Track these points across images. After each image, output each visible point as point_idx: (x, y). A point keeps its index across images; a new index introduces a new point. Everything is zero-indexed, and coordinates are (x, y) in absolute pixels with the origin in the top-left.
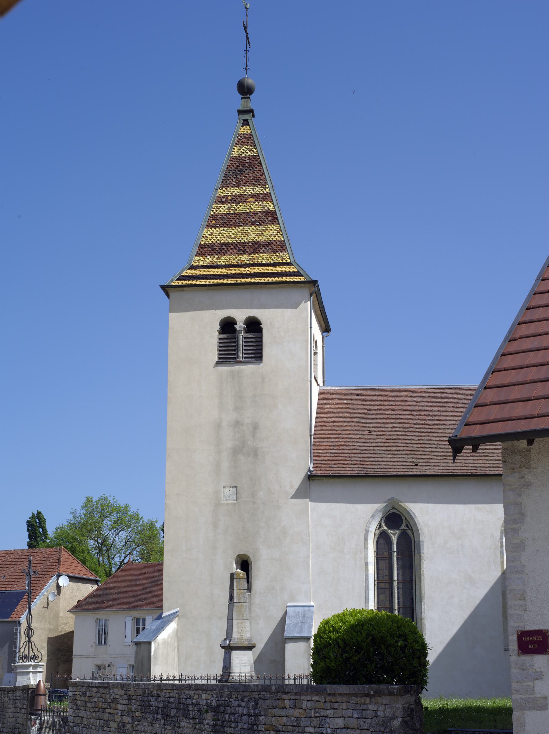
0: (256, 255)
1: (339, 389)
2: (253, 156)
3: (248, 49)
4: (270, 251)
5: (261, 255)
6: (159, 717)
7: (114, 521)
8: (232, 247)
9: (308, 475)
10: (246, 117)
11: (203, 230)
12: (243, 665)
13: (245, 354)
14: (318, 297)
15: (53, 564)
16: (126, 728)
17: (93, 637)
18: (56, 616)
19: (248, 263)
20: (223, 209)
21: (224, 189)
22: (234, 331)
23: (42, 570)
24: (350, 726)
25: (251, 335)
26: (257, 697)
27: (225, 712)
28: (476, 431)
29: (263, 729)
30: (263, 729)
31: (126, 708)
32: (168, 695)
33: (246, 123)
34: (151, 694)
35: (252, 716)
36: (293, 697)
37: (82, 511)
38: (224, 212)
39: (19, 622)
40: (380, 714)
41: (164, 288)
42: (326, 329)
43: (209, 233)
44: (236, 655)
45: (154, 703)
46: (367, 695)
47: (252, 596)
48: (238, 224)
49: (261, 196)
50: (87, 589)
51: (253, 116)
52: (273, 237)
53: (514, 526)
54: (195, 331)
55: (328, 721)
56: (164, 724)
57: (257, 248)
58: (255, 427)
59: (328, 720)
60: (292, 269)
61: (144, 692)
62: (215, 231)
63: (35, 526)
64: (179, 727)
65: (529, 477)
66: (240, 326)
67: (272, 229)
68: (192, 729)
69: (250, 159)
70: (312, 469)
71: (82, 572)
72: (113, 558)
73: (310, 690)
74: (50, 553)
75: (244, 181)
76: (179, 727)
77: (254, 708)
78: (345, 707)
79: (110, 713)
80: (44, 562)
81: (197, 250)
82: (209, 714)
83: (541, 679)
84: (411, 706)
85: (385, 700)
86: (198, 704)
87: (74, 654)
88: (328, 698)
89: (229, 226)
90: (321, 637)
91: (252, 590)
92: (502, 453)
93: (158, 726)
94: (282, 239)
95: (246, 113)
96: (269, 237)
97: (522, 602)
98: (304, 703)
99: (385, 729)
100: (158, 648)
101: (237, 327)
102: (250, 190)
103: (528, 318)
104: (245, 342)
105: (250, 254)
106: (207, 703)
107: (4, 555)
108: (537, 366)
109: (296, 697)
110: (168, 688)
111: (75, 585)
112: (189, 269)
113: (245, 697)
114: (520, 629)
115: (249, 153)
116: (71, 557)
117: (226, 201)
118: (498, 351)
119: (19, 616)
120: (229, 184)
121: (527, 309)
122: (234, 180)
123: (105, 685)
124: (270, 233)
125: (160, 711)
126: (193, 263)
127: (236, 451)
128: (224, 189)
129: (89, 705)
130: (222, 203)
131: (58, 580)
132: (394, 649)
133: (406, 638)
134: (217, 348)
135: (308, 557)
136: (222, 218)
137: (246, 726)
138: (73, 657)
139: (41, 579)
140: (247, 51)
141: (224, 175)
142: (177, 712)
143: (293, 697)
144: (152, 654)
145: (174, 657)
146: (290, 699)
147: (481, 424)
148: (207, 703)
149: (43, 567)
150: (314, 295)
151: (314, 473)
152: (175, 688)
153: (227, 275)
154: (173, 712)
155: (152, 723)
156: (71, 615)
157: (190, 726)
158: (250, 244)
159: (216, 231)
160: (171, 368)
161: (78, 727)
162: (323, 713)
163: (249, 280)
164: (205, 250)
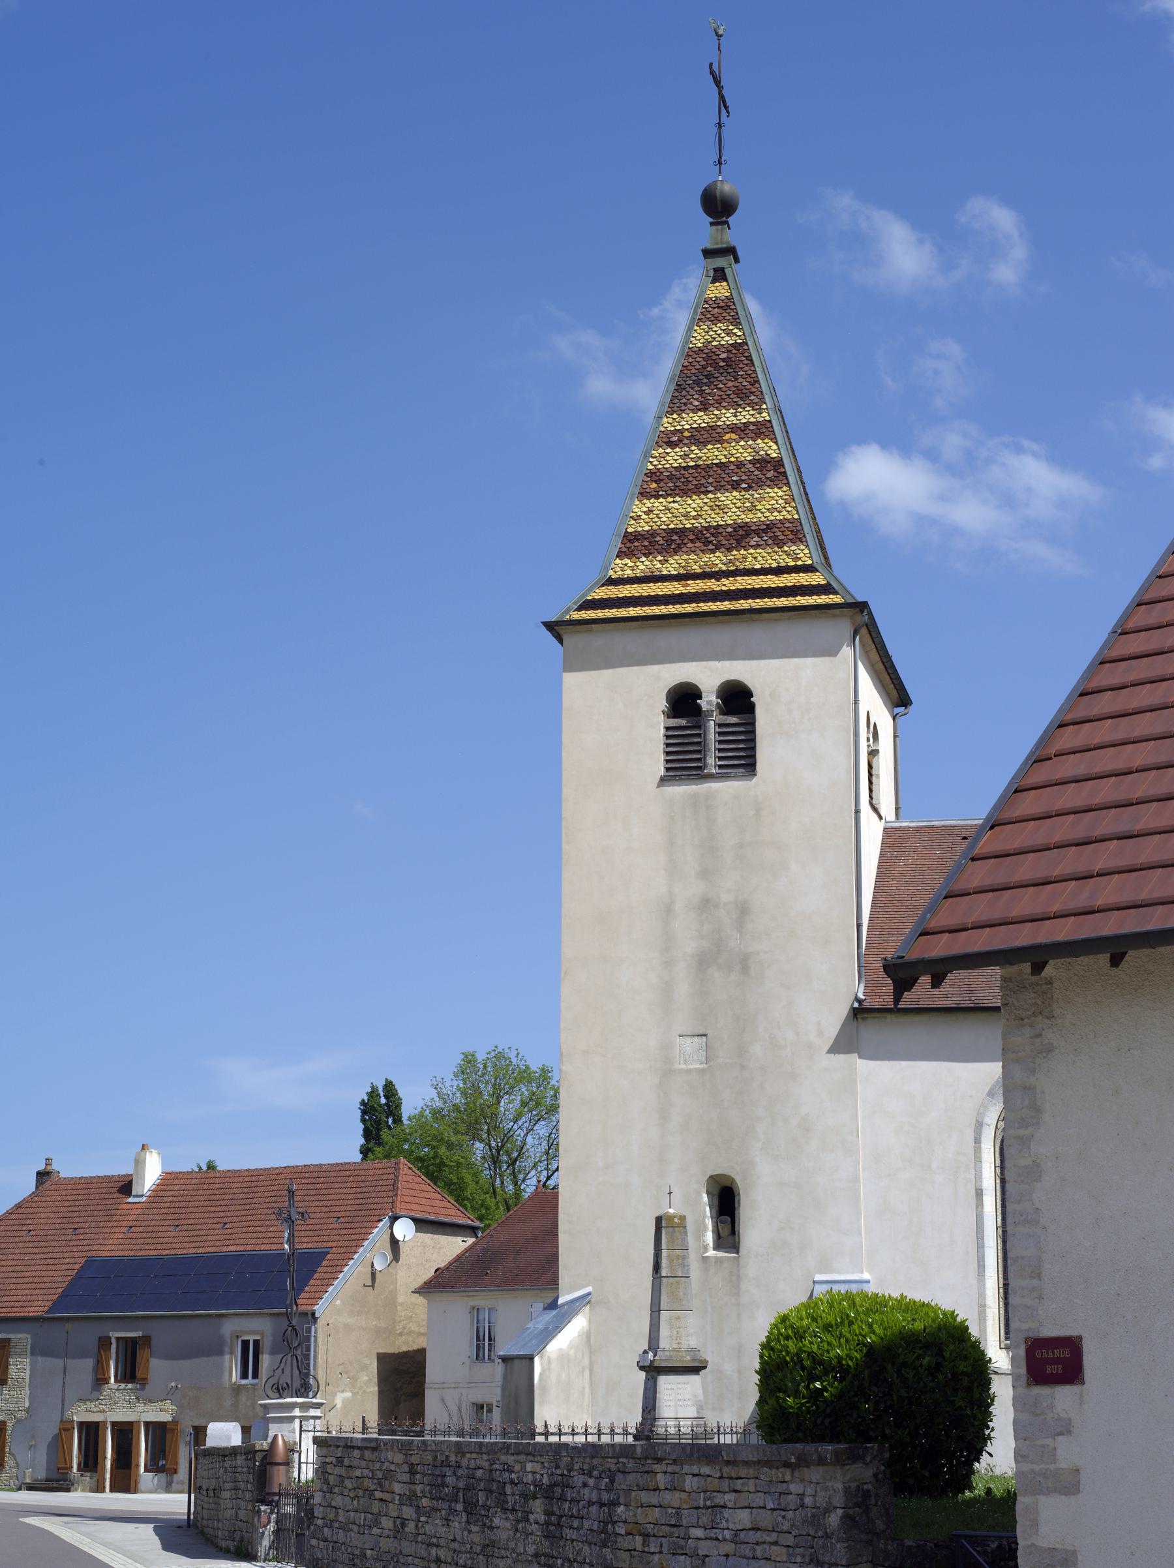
0: (742, 552)
1: (922, 827)
2: (735, 346)
3: (724, 119)
4: (770, 542)
5: (752, 551)
6: (460, 1507)
7: (522, 1100)
8: (692, 537)
9: (854, 1009)
10: (720, 262)
11: (632, 503)
12: (681, 1403)
13: (720, 758)
14: (874, 635)
15: (383, 1194)
16: (407, 1530)
17: (464, 1344)
18: (391, 1302)
19: (724, 568)
20: (674, 458)
21: (675, 416)
22: (696, 712)
23: (361, 1207)
24: (762, 1525)
25: (732, 719)
26: (614, 1468)
27: (562, 1498)
28: (940, 947)
29: (623, 1532)
30: (623, 1532)
31: (405, 1489)
32: (473, 1465)
33: (719, 275)
34: (446, 1463)
35: (605, 1505)
36: (670, 1469)
37: (455, 1083)
38: (676, 465)
39: (313, 1314)
40: (808, 1501)
41: (551, 626)
42: (898, 697)
43: (645, 509)
44: (666, 1383)
45: (450, 1480)
46: (787, 1465)
47: (742, 1262)
48: (703, 489)
49: (751, 427)
50: (454, 1246)
51: (737, 260)
52: (776, 514)
53: (1021, 1132)
54: (616, 710)
55: (726, 1515)
56: (468, 1522)
57: (743, 537)
58: (743, 910)
59: (726, 1513)
60: (817, 579)
61: (435, 1458)
62: (656, 504)
63: (379, 1112)
64: (491, 1528)
65: (1050, 1036)
66: (709, 700)
67: (776, 494)
68: (511, 1532)
69: (729, 351)
70: (861, 996)
71: (442, 1211)
72: (524, 1180)
73: (696, 1455)
74: (377, 1172)
75: (717, 398)
76: (491, 1528)
77: (609, 1490)
78: (752, 1489)
79: (381, 1500)
80: (365, 1190)
81: (620, 545)
82: (538, 1502)
83: (1069, 1432)
84: (865, 1487)
85: (815, 1473)
86: (521, 1482)
87: (428, 1380)
88: (727, 1470)
89: (685, 493)
90: (772, 1349)
91: (741, 1249)
92: (1002, 987)
93: (457, 1525)
94: (796, 516)
95: (720, 259)
96: (768, 514)
97: (1035, 1282)
98: (688, 1478)
99: (816, 1532)
100: (549, 1369)
101: (703, 703)
102: (728, 417)
103: (1079, 714)
104: (720, 734)
105: (729, 550)
106: (535, 1480)
107: (282, 1176)
108: (1075, 813)
109: (676, 1468)
110: (472, 1449)
111: (427, 1238)
112: (603, 585)
113: (594, 1468)
114: (1031, 1335)
115: (727, 338)
116: (419, 1180)
117: (680, 441)
118: (1009, 784)
119: (313, 1301)
120: (685, 404)
121: (1081, 695)
122: (696, 396)
123: (373, 1445)
124: (772, 505)
125: (461, 1495)
126: (611, 573)
127: (704, 962)
128: (675, 416)
129: (348, 1483)
130: (672, 445)
131: (391, 1227)
132: (912, 1374)
133: (941, 1350)
134: (662, 747)
135: (856, 1179)
136: (670, 477)
137: (595, 1527)
138: (426, 1386)
139: (357, 1225)
140: (720, 125)
141: (673, 386)
142: (487, 1499)
143: (670, 1469)
144: (536, 1381)
145: (584, 1388)
146: (665, 1473)
147: (950, 932)
148: (535, 1480)
149: (361, 1201)
150: (864, 631)
151: (866, 1005)
152: (484, 1449)
153: (681, 595)
154: (482, 1497)
155: (448, 1520)
156: (420, 1300)
157: (508, 1525)
158: (730, 530)
159: (658, 504)
160: (569, 791)
161: (331, 1527)
162: (719, 1499)
163: (726, 605)
164: (636, 544)
